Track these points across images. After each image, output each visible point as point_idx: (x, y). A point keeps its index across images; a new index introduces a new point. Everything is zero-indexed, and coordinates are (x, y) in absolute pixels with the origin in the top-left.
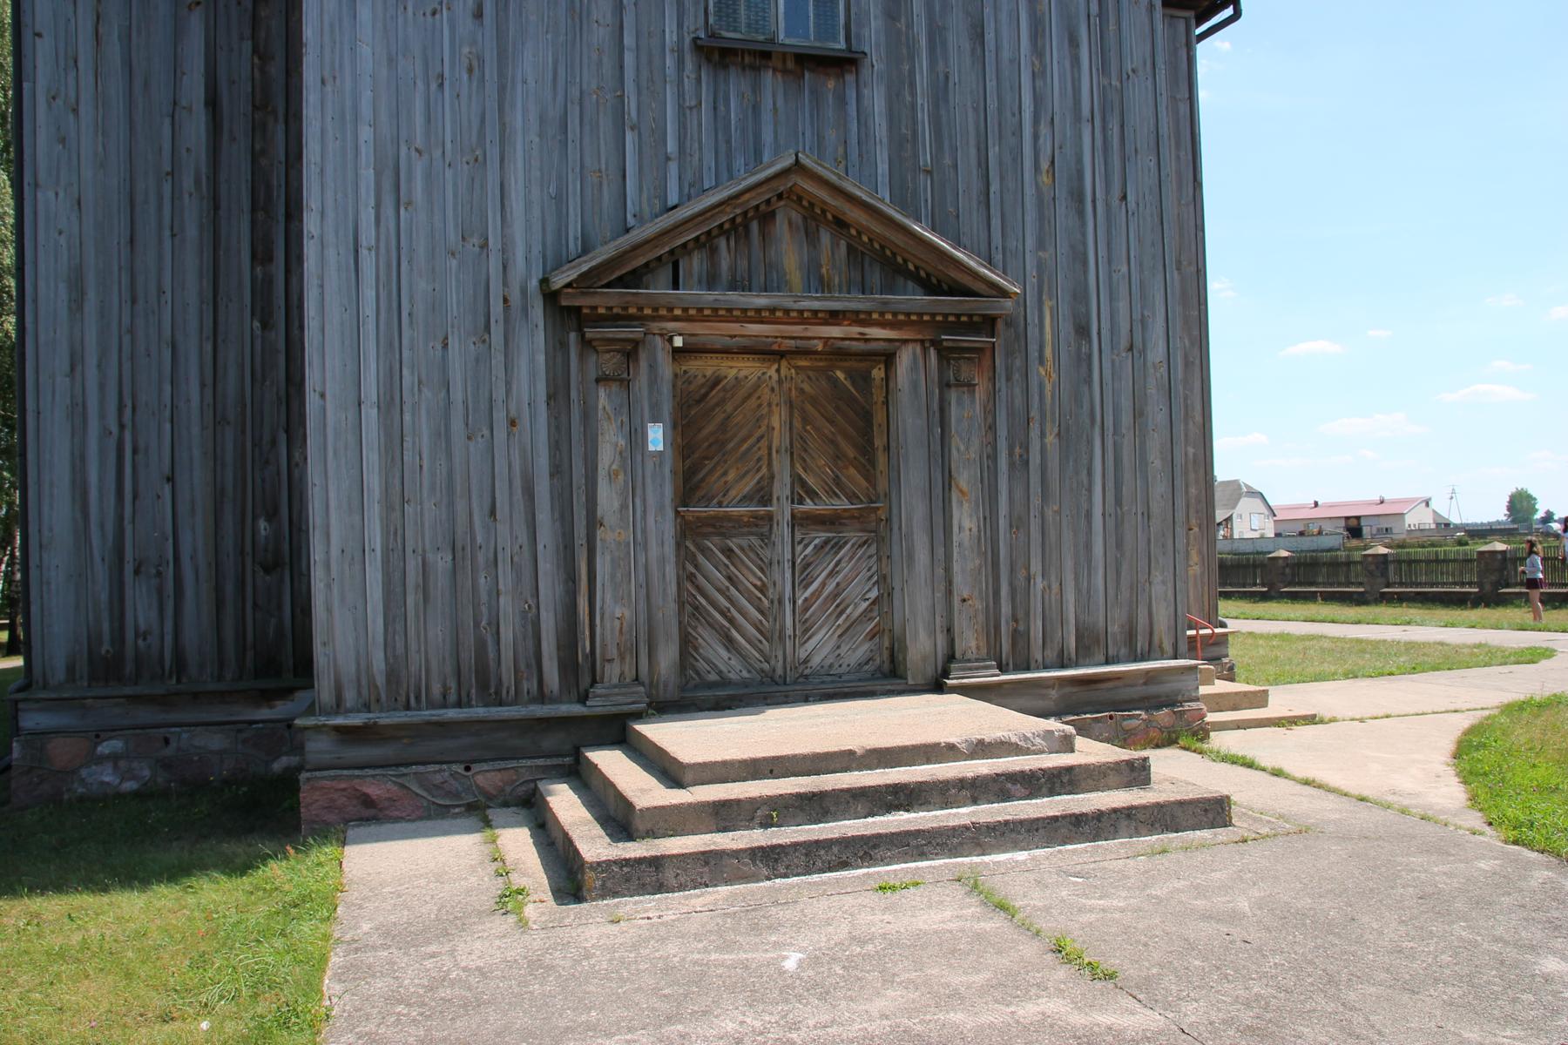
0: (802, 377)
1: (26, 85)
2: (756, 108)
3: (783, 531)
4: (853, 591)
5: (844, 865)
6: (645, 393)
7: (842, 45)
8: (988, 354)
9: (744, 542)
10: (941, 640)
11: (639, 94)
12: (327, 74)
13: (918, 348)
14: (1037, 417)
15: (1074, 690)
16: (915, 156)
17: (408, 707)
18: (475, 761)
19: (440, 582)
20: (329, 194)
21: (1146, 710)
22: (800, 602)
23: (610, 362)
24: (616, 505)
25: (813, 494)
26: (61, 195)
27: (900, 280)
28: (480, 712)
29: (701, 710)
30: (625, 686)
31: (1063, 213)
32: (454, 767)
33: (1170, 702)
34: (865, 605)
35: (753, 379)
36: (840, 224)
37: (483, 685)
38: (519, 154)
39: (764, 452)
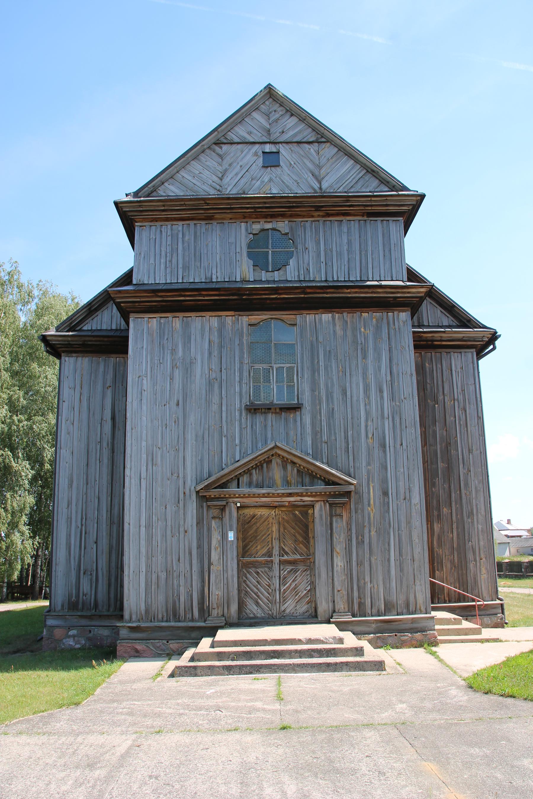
0: (284, 513)
1: (59, 417)
2: (266, 426)
3: (276, 567)
4: (302, 587)
5: (251, 673)
6: (228, 521)
7: (296, 402)
8: (349, 503)
9: (263, 570)
10: (331, 605)
11: (227, 425)
12: (133, 427)
13: (322, 503)
14: (367, 526)
15: (382, 624)
16: (321, 437)
17: (151, 621)
18: (170, 640)
19: (163, 582)
20: (133, 463)
21: (411, 633)
22: (282, 590)
23: (215, 512)
24: (217, 558)
25: (287, 553)
26: (68, 450)
27: (316, 480)
28: (172, 624)
29: (245, 626)
30: (219, 617)
31: (377, 452)
32: (163, 641)
33: (422, 630)
34: (305, 592)
35: (266, 515)
36: (294, 463)
37: (175, 615)
38: (190, 447)
39: (270, 539)
